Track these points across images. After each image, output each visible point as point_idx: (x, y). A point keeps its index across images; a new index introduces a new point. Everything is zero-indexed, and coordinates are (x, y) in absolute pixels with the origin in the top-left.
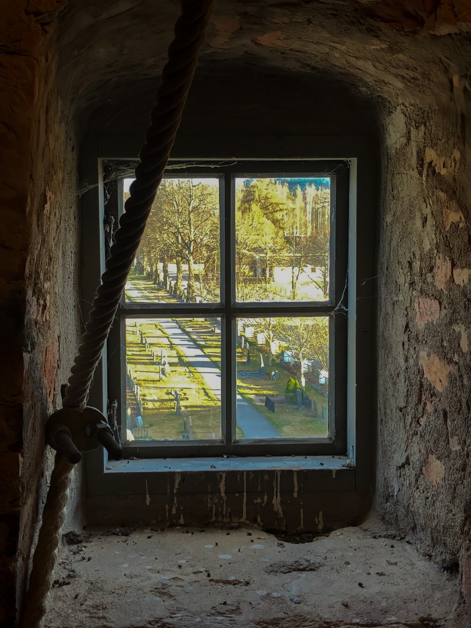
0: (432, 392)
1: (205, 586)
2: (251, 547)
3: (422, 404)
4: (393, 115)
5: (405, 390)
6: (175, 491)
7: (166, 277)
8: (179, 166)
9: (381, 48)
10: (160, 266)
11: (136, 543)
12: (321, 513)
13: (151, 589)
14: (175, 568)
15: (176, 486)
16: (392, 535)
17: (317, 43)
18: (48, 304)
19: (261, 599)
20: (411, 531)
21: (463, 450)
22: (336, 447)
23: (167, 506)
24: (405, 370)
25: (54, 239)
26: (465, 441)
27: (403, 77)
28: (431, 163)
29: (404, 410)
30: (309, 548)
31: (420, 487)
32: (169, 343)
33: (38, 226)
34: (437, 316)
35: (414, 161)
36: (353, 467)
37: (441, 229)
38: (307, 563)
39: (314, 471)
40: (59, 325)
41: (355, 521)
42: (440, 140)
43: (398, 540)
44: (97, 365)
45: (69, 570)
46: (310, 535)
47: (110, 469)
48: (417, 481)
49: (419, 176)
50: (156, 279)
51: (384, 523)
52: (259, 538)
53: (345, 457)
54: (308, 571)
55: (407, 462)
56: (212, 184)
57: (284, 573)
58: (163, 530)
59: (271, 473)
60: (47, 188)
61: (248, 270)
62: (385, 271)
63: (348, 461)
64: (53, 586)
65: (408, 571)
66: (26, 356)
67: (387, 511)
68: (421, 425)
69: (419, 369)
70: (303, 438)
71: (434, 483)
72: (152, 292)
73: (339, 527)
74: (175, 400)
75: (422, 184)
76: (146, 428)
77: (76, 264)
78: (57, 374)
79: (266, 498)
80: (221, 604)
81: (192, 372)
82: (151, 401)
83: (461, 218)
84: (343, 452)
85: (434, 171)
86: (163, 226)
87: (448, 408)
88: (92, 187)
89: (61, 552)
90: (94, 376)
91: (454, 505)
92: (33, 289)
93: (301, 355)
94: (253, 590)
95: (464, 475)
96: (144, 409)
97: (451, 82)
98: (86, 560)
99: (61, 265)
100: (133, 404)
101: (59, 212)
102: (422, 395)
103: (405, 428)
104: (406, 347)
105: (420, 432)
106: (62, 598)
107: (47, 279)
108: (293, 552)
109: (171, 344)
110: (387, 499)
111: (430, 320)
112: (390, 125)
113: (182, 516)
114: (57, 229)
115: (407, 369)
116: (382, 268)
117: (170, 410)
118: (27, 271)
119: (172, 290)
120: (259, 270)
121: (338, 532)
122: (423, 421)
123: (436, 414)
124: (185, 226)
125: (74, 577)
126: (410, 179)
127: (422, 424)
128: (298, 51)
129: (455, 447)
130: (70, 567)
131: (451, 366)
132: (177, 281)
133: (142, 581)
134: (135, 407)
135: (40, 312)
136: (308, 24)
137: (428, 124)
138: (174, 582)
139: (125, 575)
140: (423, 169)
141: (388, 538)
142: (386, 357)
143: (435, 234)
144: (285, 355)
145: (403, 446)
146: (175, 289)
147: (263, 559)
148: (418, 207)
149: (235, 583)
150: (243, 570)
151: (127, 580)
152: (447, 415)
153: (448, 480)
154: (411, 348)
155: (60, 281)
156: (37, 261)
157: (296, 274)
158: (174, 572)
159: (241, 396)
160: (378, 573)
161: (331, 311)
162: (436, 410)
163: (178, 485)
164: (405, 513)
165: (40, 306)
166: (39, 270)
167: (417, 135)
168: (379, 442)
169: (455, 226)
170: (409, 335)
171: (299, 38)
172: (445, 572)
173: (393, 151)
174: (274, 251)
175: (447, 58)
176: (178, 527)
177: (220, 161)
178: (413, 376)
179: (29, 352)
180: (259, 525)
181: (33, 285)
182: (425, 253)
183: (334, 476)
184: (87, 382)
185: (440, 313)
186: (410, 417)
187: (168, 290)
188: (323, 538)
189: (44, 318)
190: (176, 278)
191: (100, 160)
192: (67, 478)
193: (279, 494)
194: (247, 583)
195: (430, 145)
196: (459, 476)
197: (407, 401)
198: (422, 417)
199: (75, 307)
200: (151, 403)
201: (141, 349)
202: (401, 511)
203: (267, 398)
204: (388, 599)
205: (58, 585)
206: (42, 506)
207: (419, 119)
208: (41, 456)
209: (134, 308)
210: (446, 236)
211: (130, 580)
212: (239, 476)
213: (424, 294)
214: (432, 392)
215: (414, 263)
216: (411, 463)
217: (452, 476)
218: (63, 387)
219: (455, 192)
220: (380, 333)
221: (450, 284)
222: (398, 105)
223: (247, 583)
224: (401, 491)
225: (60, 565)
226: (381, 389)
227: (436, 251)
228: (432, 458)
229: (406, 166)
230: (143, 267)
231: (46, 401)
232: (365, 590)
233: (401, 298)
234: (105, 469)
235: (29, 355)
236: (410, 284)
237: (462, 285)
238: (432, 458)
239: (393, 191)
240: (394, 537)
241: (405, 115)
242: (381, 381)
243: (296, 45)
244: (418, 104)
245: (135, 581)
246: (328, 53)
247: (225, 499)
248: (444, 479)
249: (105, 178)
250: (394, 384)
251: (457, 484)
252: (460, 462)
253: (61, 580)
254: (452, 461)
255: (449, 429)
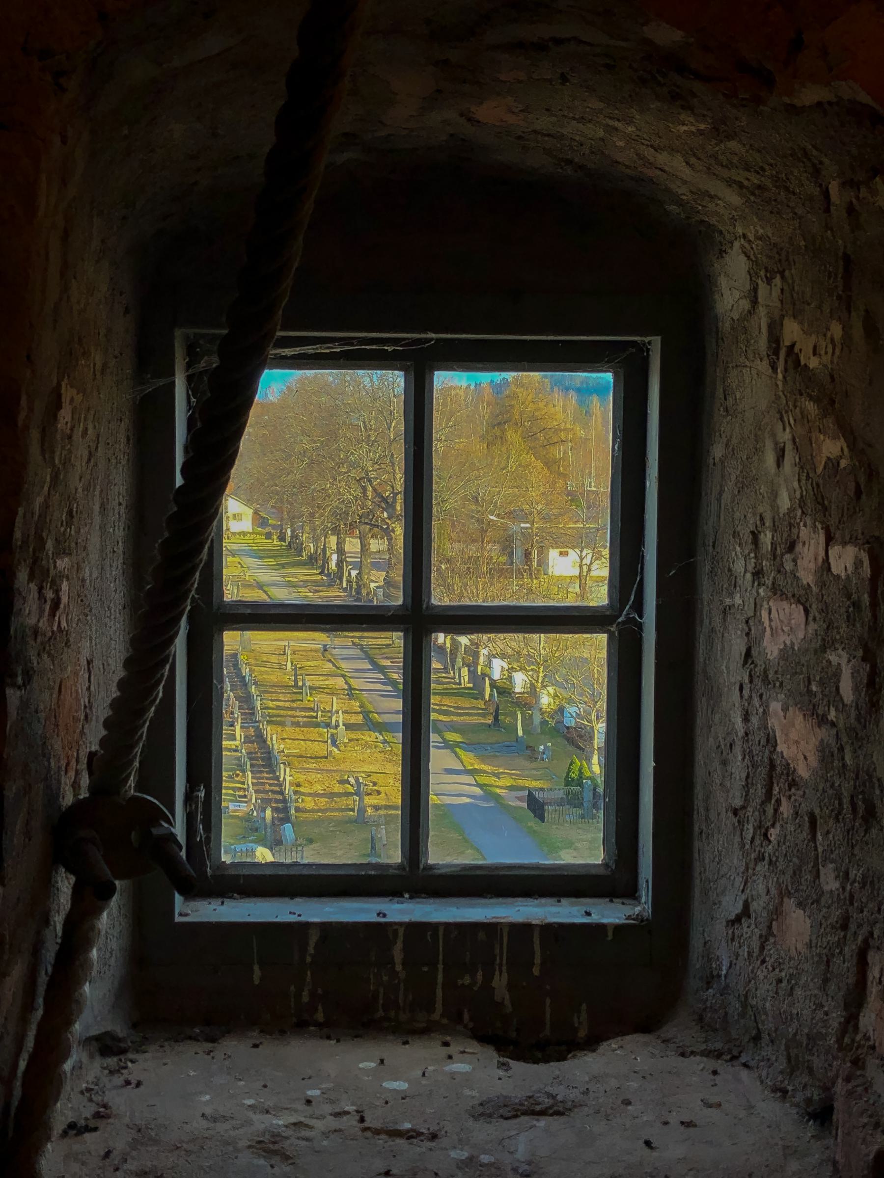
0: (790, 778)
1: (352, 1139)
2: (447, 1068)
3: (773, 801)
4: (727, 258)
5: (744, 775)
6: (309, 959)
7: (342, 563)
8: (328, 348)
9: (698, 130)
10: (333, 540)
11: (229, 1057)
12: (584, 1007)
13: (249, 1143)
14: (301, 1106)
15: (311, 950)
16: (715, 1051)
17: (582, 120)
18: (64, 599)
19: (458, 1167)
20: (752, 1045)
21: (844, 889)
22: (612, 882)
23: (292, 988)
24: (743, 738)
25: (81, 478)
26: (847, 874)
27: (741, 186)
28: (793, 346)
29: (741, 813)
30: (557, 1072)
31: (767, 959)
32: (346, 687)
33: (43, 452)
34: (801, 635)
35: (763, 343)
36: (647, 920)
37: (810, 471)
38: (551, 1101)
39: (573, 925)
40: (91, 639)
41: (648, 1023)
42: (809, 304)
43: (726, 1061)
44: (151, 715)
45: (98, 1104)
46: (564, 1048)
47: (186, 915)
48: (762, 948)
49: (770, 371)
50: (323, 567)
51: (702, 1027)
52: (463, 1052)
53: (633, 902)
54: (551, 1115)
55: (746, 911)
56: (393, 382)
57: (507, 1118)
58: (283, 1032)
59: (491, 928)
60: (66, 380)
61: (497, 552)
62: (711, 549)
63: (638, 909)
64: (65, 1134)
65: (740, 1119)
66: (13, 696)
67: (708, 1004)
68: (770, 841)
69: (768, 735)
70: (554, 864)
71: (793, 953)
72: (317, 591)
73: (617, 1035)
74: (356, 794)
75: (777, 385)
76: (300, 845)
77: (129, 527)
78: (82, 733)
79: (479, 976)
80: (380, 1174)
81: (389, 743)
82: (310, 795)
83: (842, 449)
84: (630, 893)
85: (797, 362)
86: (339, 467)
87: (819, 809)
88: (162, 382)
89: (79, 1068)
90: (147, 736)
91: (827, 995)
92: (31, 568)
93: (594, 714)
94: (442, 1149)
95: (845, 937)
96: (297, 810)
97: (826, 194)
98: (133, 1085)
99: (97, 528)
100: (277, 801)
101: (95, 427)
102: (772, 783)
103: (743, 846)
104: (746, 692)
105: (770, 855)
106: (80, 1157)
107: (62, 551)
108: (525, 1078)
109: (351, 688)
110: (708, 983)
111: (788, 643)
112: (722, 275)
113: (320, 1008)
114: (89, 460)
115: (747, 734)
116: (704, 545)
117: (344, 814)
118: (18, 534)
119: (351, 587)
120: (518, 554)
121: (614, 1044)
122: (774, 833)
123: (797, 821)
124: (383, 466)
125: (108, 1117)
126: (755, 376)
127: (772, 839)
128: (549, 135)
129: (830, 882)
130: (100, 1098)
131: (824, 730)
132: (360, 569)
133: (234, 1128)
134: (280, 805)
135: (46, 613)
136: (563, 84)
137: (787, 273)
138: (295, 1131)
139: (203, 1115)
140: (778, 359)
141: (707, 1056)
142: (709, 712)
143: (799, 481)
144: (566, 714)
145: (739, 881)
146: (359, 586)
147: (467, 1092)
148: (768, 429)
149: (411, 1135)
150: (429, 1111)
151: (204, 1124)
152: (816, 823)
153: (816, 946)
154: (754, 695)
155: (94, 556)
156: (40, 516)
157: (587, 561)
158: (296, 1111)
159: (482, 789)
160: (682, 1123)
161: (611, 624)
162: (797, 813)
163: (315, 948)
164: (740, 1009)
165: (46, 601)
166: (44, 534)
167: (770, 295)
168: (696, 874)
169: (833, 464)
170: (751, 670)
171: (547, 110)
172: (811, 1122)
173: (727, 324)
174: (546, 519)
175: (817, 149)
176: (312, 1028)
177: (404, 339)
178: (758, 748)
179: (19, 688)
180: (465, 1026)
181: (30, 561)
182: (781, 515)
183: (610, 937)
184: (132, 747)
185: (806, 629)
186: (750, 827)
187: (345, 586)
188: (585, 1055)
189: (56, 624)
190: (359, 566)
191: (178, 333)
192: (93, 928)
193: (504, 969)
194: (434, 1137)
195: (790, 312)
196: (836, 939)
197: (746, 795)
198: (773, 826)
199: (124, 608)
200: (310, 799)
201: (295, 697)
202: (735, 1006)
203: (530, 794)
204: (698, 1171)
205: (75, 1132)
206: (43, 980)
207: (772, 264)
208: (44, 887)
209: (240, 612)
210: (818, 485)
211: (213, 1125)
212: (429, 933)
213: (779, 592)
214: (790, 778)
215: (762, 534)
216: (753, 915)
217: (824, 939)
218: (91, 755)
219: (832, 402)
220: (699, 668)
221: (822, 575)
222: (736, 239)
223: (434, 1137)
224: (733, 966)
225: (82, 1093)
226: (700, 772)
227: (799, 513)
228: (790, 904)
229: (749, 352)
230: (302, 544)
231: (59, 782)
232: (655, 1154)
233: (738, 601)
234: (176, 915)
235: (18, 693)
236: (753, 574)
237: (843, 575)
238: (790, 904)
239: (726, 399)
240: (718, 1055)
241: (748, 257)
242: (700, 757)
243: (543, 122)
244: (770, 235)
245: (221, 1127)
246: (602, 140)
247: (402, 975)
248: (809, 945)
249: (189, 366)
250: (724, 763)
251: (833, 955)
252: (837, 913)
253: (83, 1123)
254: (824, 910)
255: (820, 850)
